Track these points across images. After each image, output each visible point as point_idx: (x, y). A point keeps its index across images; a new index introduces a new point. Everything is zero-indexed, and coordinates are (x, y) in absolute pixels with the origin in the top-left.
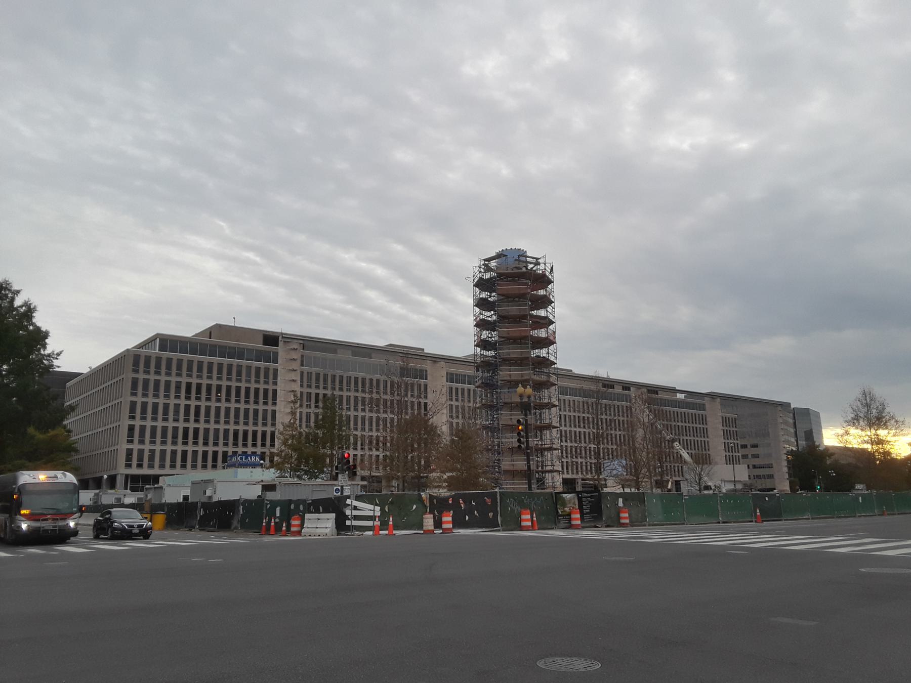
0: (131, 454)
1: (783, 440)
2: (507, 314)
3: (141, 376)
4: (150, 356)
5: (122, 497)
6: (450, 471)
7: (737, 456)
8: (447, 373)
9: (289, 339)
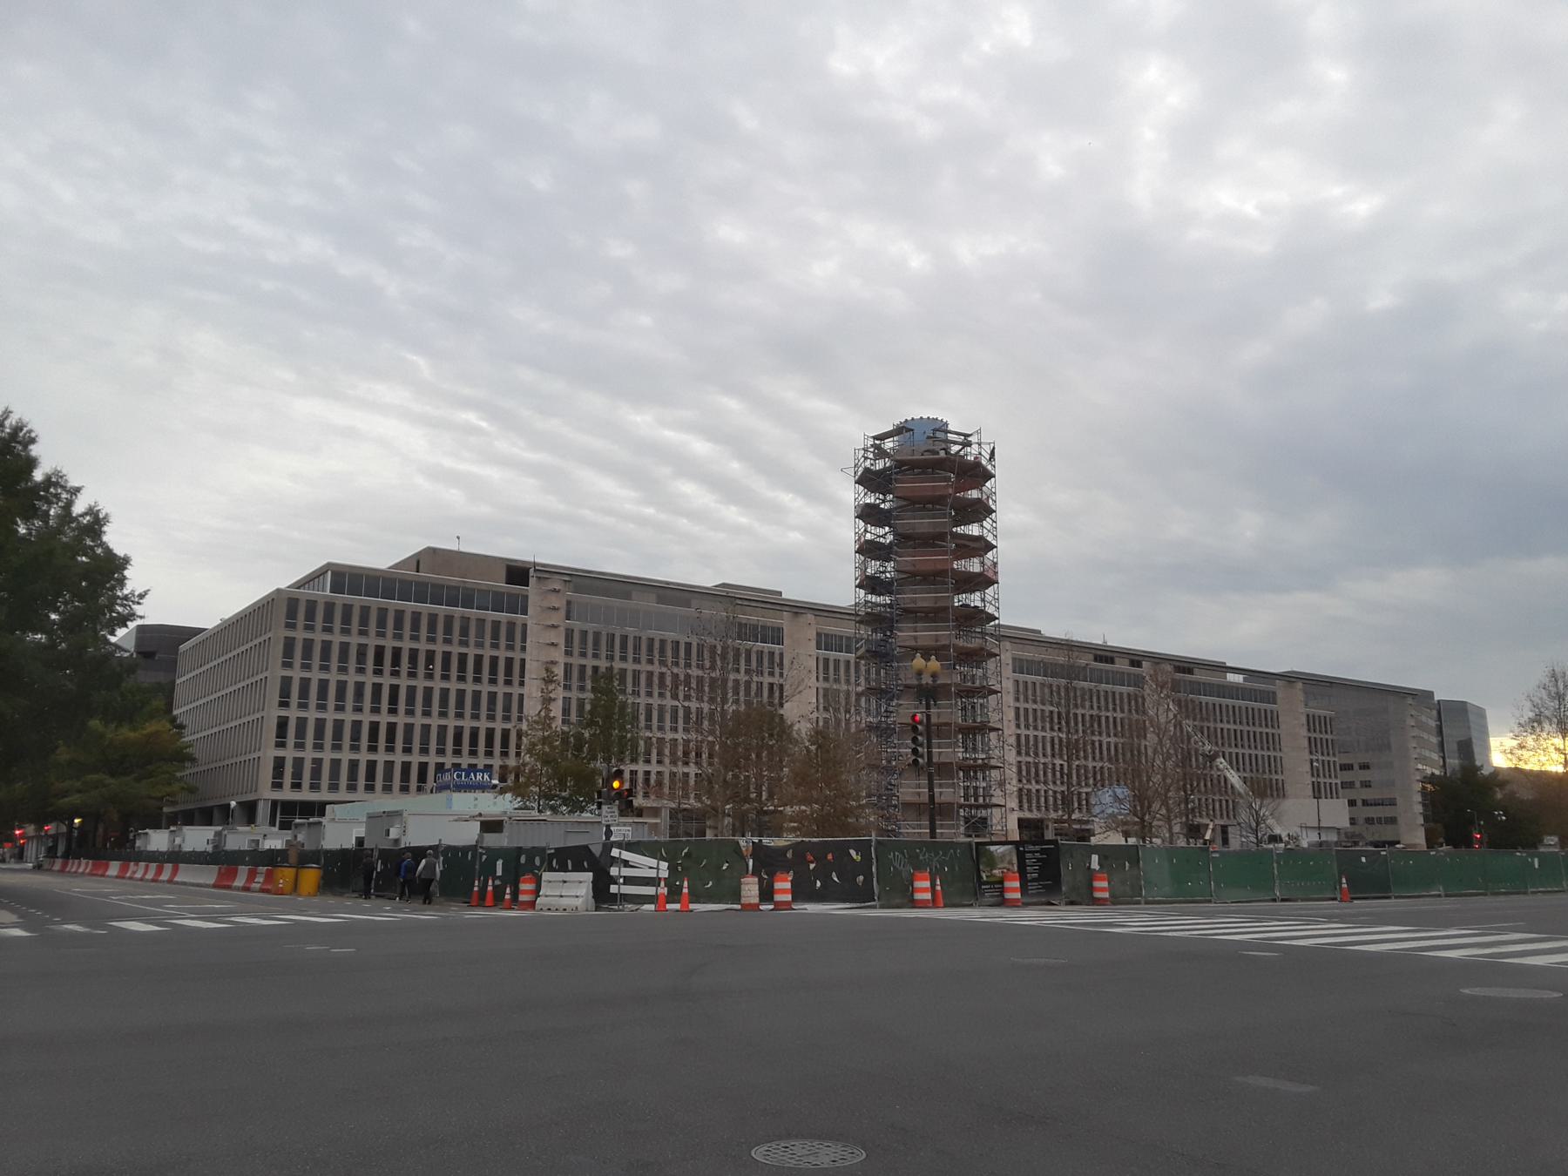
0: (283, 767)
1: (1416, 756)
2: (911, 531)
3: (300, 635)
4: (316, 601)
5: (260, 838)
6: (800, 803)
7: (1328, 784)
8: (819, 635)
9: (547, 572)
